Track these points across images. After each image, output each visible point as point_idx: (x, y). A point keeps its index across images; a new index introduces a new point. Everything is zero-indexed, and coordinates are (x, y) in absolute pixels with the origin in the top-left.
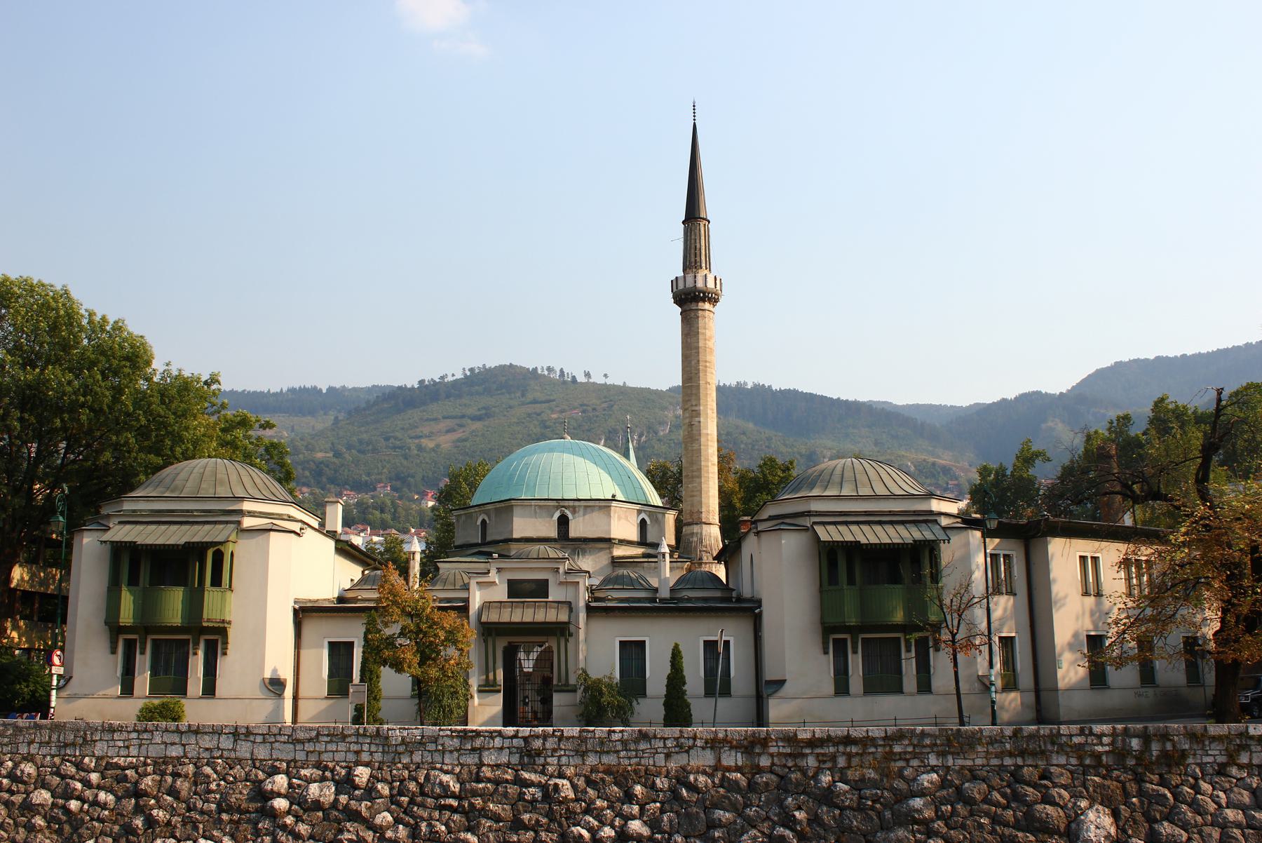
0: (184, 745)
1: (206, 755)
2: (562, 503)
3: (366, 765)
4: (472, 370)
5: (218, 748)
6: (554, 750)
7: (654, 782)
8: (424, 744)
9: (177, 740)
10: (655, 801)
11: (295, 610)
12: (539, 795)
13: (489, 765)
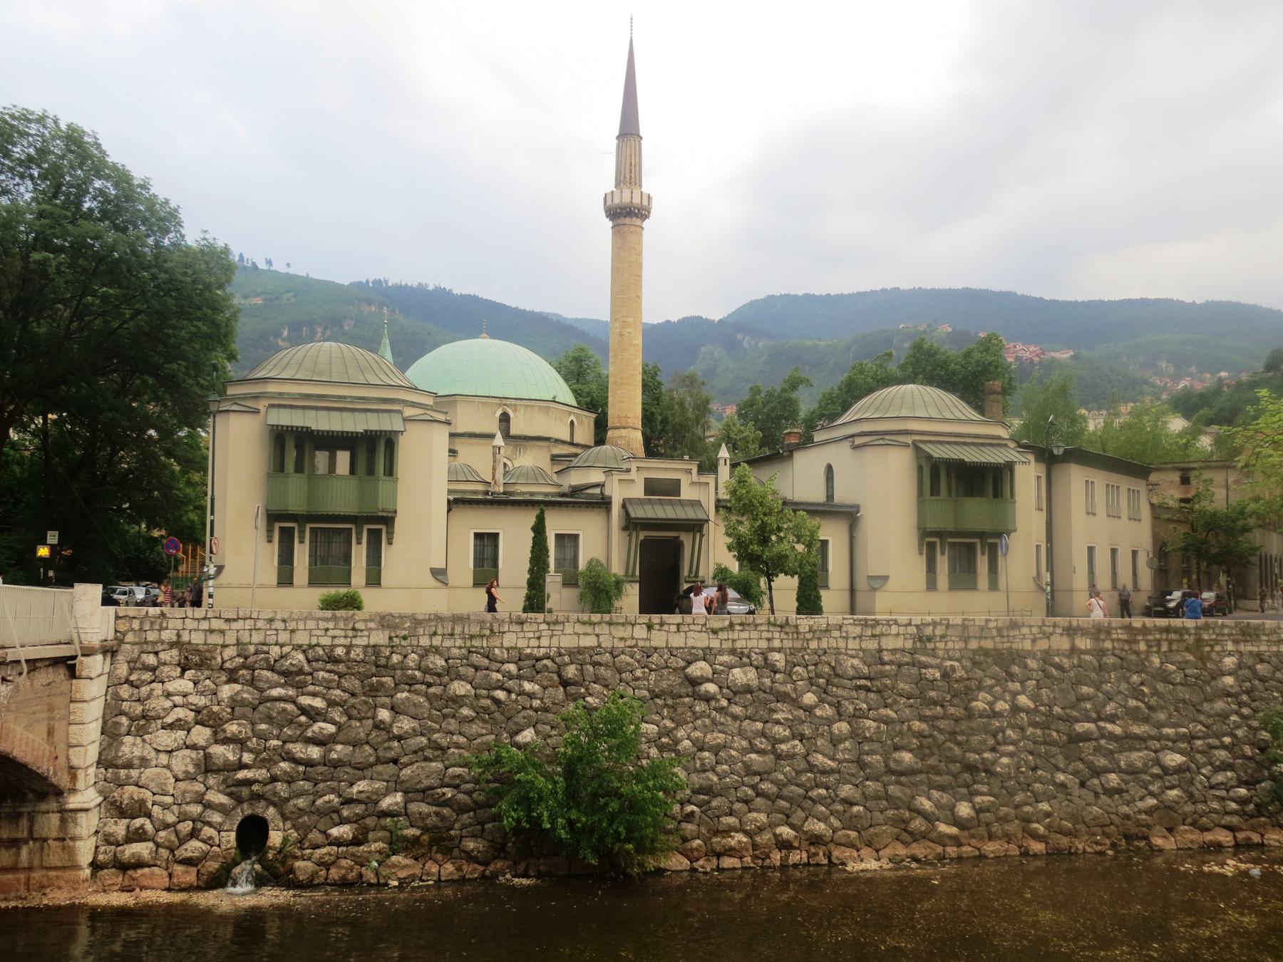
0: (597, 635)
2: (504, 401)
3: (779, 650)
5: (633, 638)
6: (943, 637)
11: (449, 501)
12: (938, 675)
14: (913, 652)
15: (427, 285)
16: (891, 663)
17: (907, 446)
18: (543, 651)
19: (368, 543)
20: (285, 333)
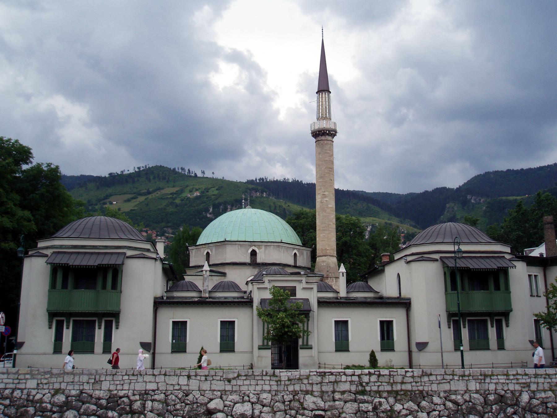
0: (157, 383)
1: (171, 388)
4: (139, 168)
5: (179, 384)
7: (432, 399)
8: (301, 380)
9: (153, 380)
10: (434, 410)
13: (339, 392)
14: (357, 393)
15: (288, 179)
16: (340, 400)
17: (437, 260)
18: (124, 392)
19: (73, 328)
20: (211, 210)
